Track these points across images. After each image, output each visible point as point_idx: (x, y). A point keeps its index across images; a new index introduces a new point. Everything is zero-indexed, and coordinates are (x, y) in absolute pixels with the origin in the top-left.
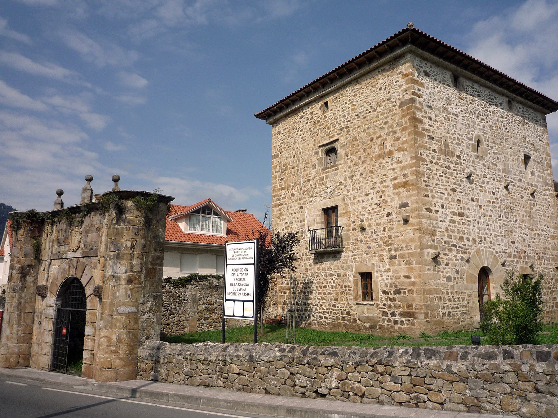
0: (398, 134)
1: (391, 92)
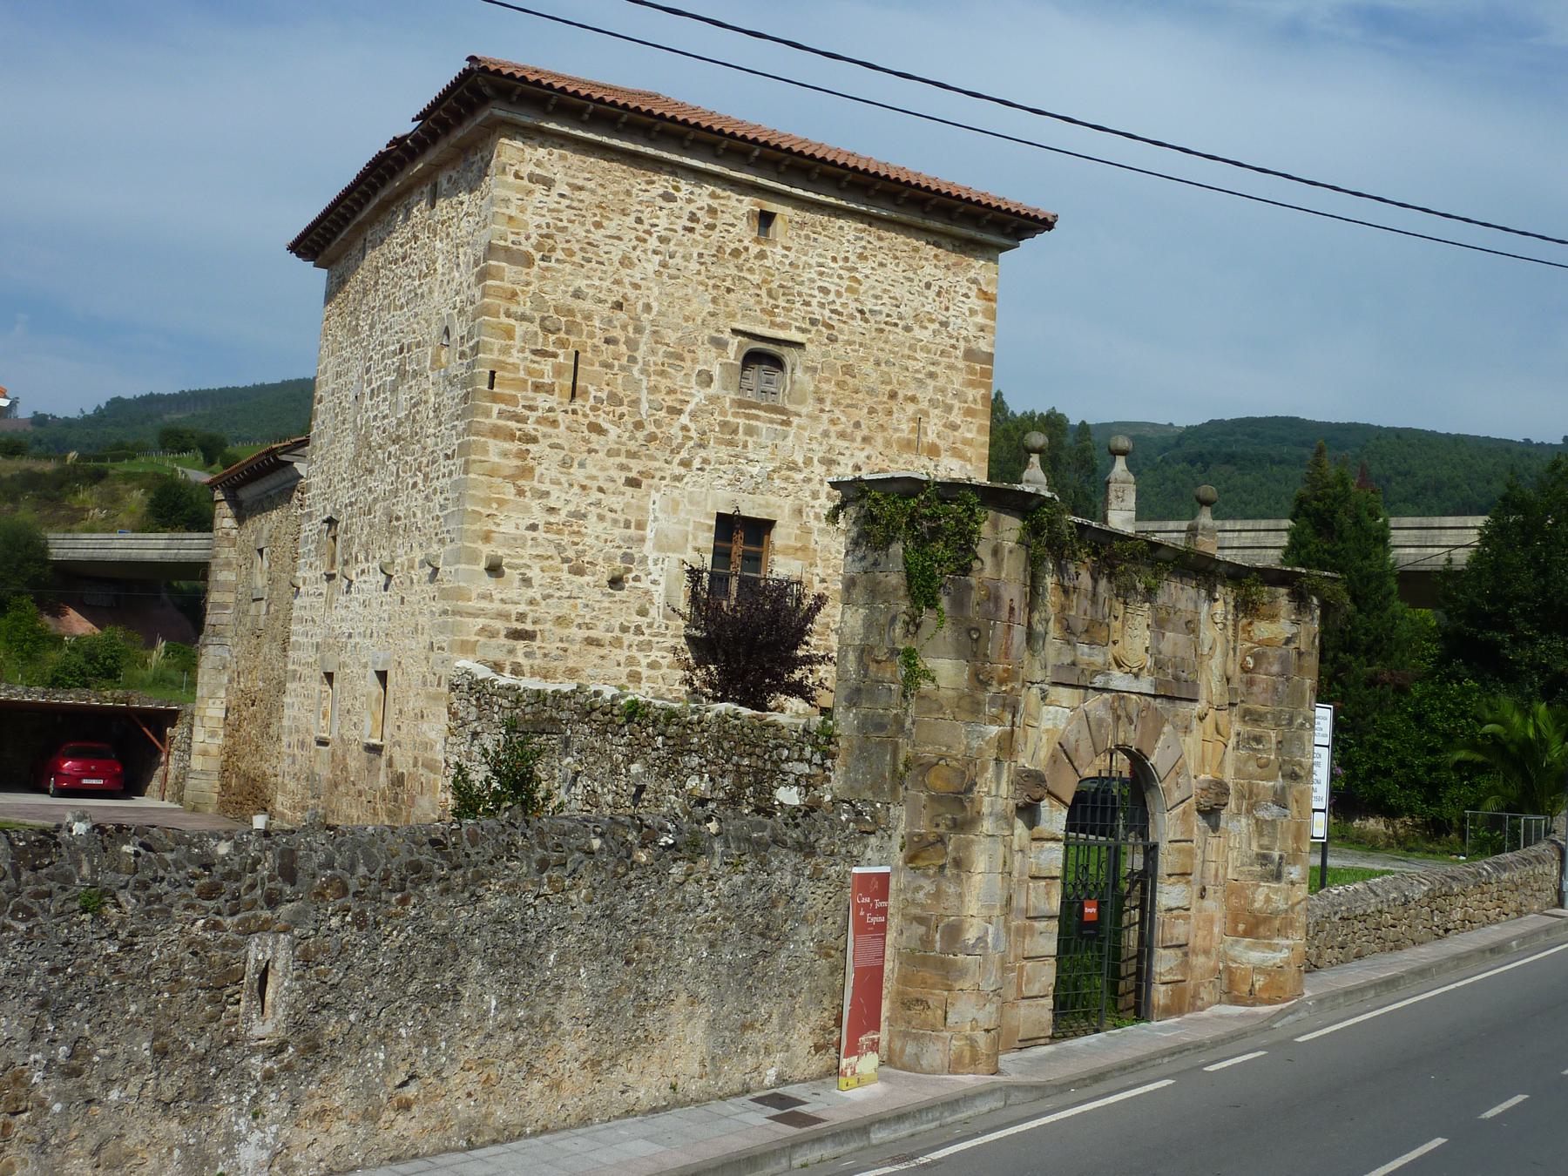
0: (956, 417)
1: (951, 312)
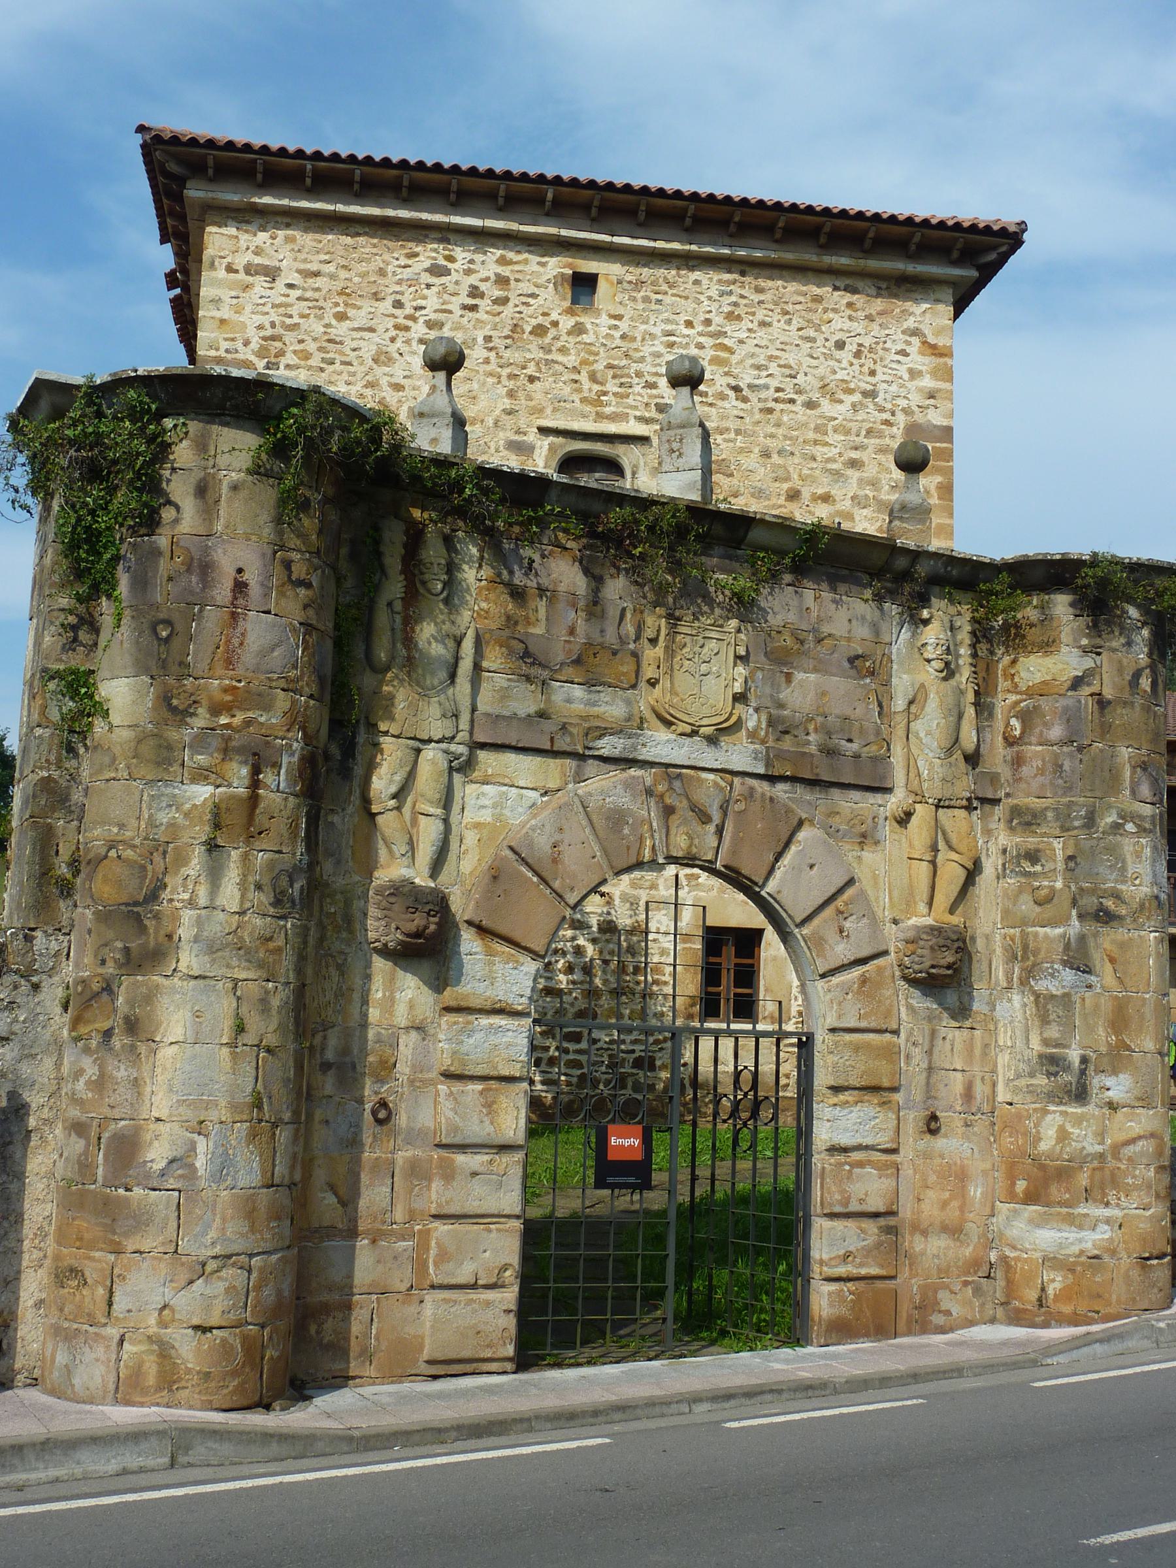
1: (880, 377)
